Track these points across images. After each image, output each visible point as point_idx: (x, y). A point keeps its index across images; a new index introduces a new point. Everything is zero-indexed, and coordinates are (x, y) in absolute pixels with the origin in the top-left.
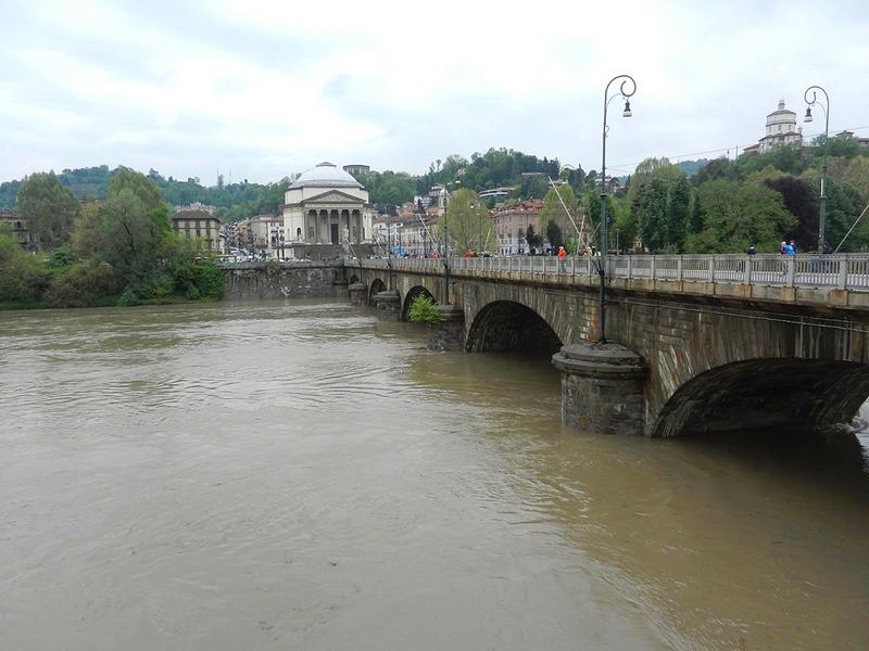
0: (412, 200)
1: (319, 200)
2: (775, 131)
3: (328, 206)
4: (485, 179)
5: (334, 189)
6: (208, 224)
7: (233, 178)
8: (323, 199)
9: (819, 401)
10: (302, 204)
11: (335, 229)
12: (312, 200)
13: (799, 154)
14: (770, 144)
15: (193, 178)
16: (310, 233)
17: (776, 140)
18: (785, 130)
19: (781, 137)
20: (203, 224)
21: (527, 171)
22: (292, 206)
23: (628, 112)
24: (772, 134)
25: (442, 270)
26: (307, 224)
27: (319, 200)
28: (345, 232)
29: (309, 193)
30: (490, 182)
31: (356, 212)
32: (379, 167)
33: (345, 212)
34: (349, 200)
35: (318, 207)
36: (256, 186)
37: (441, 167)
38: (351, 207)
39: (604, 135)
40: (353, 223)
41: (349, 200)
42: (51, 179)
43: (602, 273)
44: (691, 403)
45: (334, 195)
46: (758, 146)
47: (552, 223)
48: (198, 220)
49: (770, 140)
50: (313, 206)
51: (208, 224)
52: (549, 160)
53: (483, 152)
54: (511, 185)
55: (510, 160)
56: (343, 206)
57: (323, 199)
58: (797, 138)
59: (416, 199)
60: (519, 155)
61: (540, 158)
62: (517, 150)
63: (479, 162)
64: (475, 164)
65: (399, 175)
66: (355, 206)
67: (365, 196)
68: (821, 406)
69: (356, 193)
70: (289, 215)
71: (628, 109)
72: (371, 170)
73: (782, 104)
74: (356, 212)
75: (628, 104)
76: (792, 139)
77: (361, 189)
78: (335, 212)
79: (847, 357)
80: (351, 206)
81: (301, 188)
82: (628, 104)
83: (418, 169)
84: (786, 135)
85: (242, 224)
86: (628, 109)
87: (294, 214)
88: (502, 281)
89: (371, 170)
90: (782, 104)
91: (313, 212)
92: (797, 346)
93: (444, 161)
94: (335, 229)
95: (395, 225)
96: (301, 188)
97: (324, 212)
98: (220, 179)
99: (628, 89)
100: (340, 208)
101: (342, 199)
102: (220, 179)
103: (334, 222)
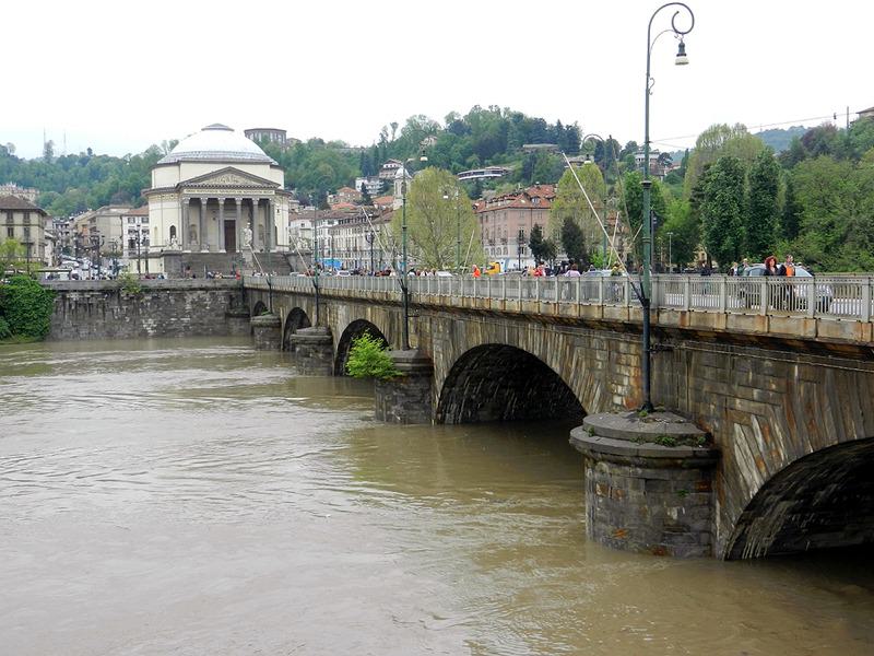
0: (352, 184)
1: (205, 183)
4: (467, 153)
6: (27, 217)
8: (212, 182)
10: (178, 188)
11: (230, 228)
12: (194, 183)
16: (190, 234)
20: (18, 218)
21: (531, 142)
22: (162, 191)
23: (682, 58)
25: (398, 296)
26: (185, 219)
27: (205, 183)
28: (245, 235)
29: (190, 172)
30: (474, 158)
31: (264, 203)
32: (301, 131)
33: (247, 202)
34: (254, 183)
35: (204, 195)
36: (105, 159)
37: (398, 134)
38: (256, 195)
40: (259, 219)
41: (254, 183)
45: (229, 176)
47: (569, 223)
48: (26, 212)
50: (196, 193)
51: (27, 217)
52: (564, 124)
53: (463, 112)
54: (505, 162)
55: (504, 126)
57: (212, 182)
59: (359, 182)
60: (519, 117)
61: (551, 121)
62: (514, 109)
63: (457, 127)
65: (333, 145)
66: (263, 194)
67: (278, 177)
69: (263, 172)
70: (158, 205)
71: (682, 52)
72: (288, 136)
74: (264, 203)
75: (682, 46)
77: (272, 166)
78: (230, 202)
80: (256, 192)
81: (178, 164)
82: (682, 46)
83: (362, 136)
86: (682, 52)
89: (288, 136)
91: (195, 202)
93: (402, 124)
94: (230, 228)
95: (326, 223)
96: (178, 164)
97: (213, 202)
98: (48, 146)
99: (683, 23)
100: (239, 195)
101: (241, 181)
102: (48, 146)
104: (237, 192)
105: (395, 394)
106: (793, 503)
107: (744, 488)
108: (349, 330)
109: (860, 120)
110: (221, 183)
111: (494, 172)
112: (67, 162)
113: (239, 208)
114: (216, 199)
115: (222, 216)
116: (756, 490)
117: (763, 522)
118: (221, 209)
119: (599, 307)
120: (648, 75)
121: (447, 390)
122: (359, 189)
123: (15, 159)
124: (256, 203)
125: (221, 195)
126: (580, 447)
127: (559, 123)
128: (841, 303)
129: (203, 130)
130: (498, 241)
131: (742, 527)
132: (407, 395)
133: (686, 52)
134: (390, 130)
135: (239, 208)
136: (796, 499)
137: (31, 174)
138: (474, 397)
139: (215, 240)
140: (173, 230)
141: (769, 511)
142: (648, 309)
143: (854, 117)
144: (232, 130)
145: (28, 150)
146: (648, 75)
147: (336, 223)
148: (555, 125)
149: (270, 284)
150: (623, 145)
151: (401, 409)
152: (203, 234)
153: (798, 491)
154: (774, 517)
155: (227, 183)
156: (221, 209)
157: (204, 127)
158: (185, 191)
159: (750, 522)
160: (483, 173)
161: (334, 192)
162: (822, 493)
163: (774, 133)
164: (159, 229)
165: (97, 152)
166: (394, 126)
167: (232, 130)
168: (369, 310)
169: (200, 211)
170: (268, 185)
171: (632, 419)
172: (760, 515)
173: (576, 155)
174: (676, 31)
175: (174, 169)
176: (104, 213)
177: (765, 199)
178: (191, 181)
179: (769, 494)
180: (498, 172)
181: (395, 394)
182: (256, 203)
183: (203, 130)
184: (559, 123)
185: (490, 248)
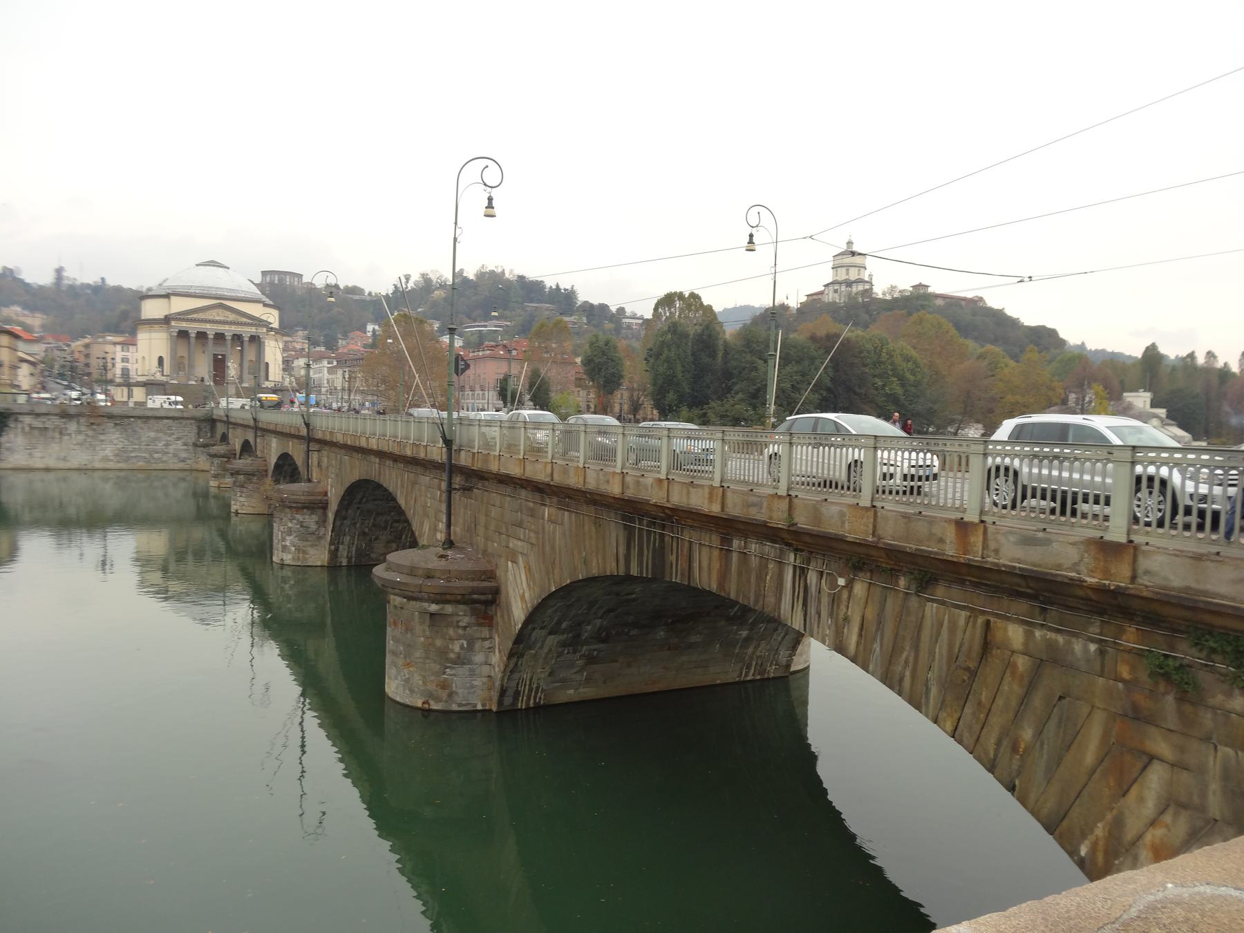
1: (195, 316)
2: (842, 275)
3: (208, 326)
5: (221, 300)
7: (83, 274)
9: (744, 633)
10: (167, 320)
12: (183, 316)
13: (866, 306)
14: (836, 291)
15: (10, 266)
16: (178, 365)
17: (843, 288)
18: (853, 275)
19: (849, 284)
21: (531, 301)
22: (152, 322)
23: (751, 246)
24: (839, 279)
25: (252, 423)
26: (173, 351)
27: (195, 316)
29: (179, 305)
31: (255, 339)
32: (316, 274)
33: (237, 338)
34: (244, 320)
35: (193, 328)
36: (118, 290)
38: (247, 331)
39: (455, 239)
40: (250, 354)
41: (244, 320)
42: (122, 288)
43: (448, 443)
44: (552, 640)
45: (220, 311)
46: (821, 293)
49: (836, 287)
50: (184, 325)
52: (562, 287)
56: (233, 328)
58: (867, 287)
60: (521, 278)
61: (550, 283)
62: (519, 271)
64: (1220, 370)
67: (273, 317)
68: (748, 640)
69: (256, 310)
71: (490, 206)
73: (850, 243)
74: (255, 339)
75: (490, 199)
76: (861, 287)
77: (265, 305)
78: (220, 337)
79: (676, 579)
81: (167, 296)
82: (490, 199)
84: (855, 282)
85: (78, 344)
86: (490, 206)
87: (154, 335)
88: (365, 452)
90: (850, 243)
91: (183, 334)
92: (632, 557)
95: (325, 363)
96: (167, 296)
97: (202, 335)
98: (59, 271)
99: (492, 176)
100: (229, 330)
101: (232, 317)
102: (59, 271)
103: (219, 350)
104: (227, 327)
105: (290, 525)
106: (562, 637)
107: (513, 623)
108: (281, 463)
109: (807, 301)
110: (210, 318)
111: (496, 326)
112: (76, 291)
113: (229, 343)
114: (224, 334)
115: (212, 349)
116: (520, 626)
117: (535, 655)
118: (193, 341)
119: (424, 446)
120: (456, 223)
121: (338, 523)
122: (369, 334)
123: (22, 281)
124: (246, 339)
125: (210, 329)
126: (379, 583)
127: (558, 286)
128: (758, 460)
129: (197, 265)
130: (478, 387)
131: (514, 660)
132: (302, 526)
133: (754, 241)
134: (404, 280)
135: (229, 343)
136: (563, 634)
137: (33, 297)
138: (367, 530)
139: (203, 368)
140: (161, 360)
141: (539, 645)
142: (451, 449)
143: (804, 299)
144: (228, 268)
145: (38, 275)
146: (456, 223)
147: (335, 363)
148: (554, 287)
149: (227, 416)
150: (614, 309)
151: (296, 541)
152: (191, 366)
153: (564, 625)
154: (546, 650)
155: (217, 318)
156: (210, 343)
157: (197, 263)
158: (173, 323)
159: (522, 656)
160: (486, 326)
161: (345, 336)
162: (589, 628)
163: (1130, 356)
164: (147, 358)
165: (111, 282)
166: (408, 278)
167: (228, 268)
168: (291, 443)
169: (189, 343)
170: (258, 322)
171: (444, 549)
172: (530, 648)
173: (571, 315)
174: (485, 185)
175: (163, 301)
176: (100, 340)
177: (705, 359)
178: (179, 314)
179: (534, 629)
180: (500, 327)
181: (290, 525)
182: (246, 339)
183: (197, 265)
184: (558, 286)
185: (470, 393)
